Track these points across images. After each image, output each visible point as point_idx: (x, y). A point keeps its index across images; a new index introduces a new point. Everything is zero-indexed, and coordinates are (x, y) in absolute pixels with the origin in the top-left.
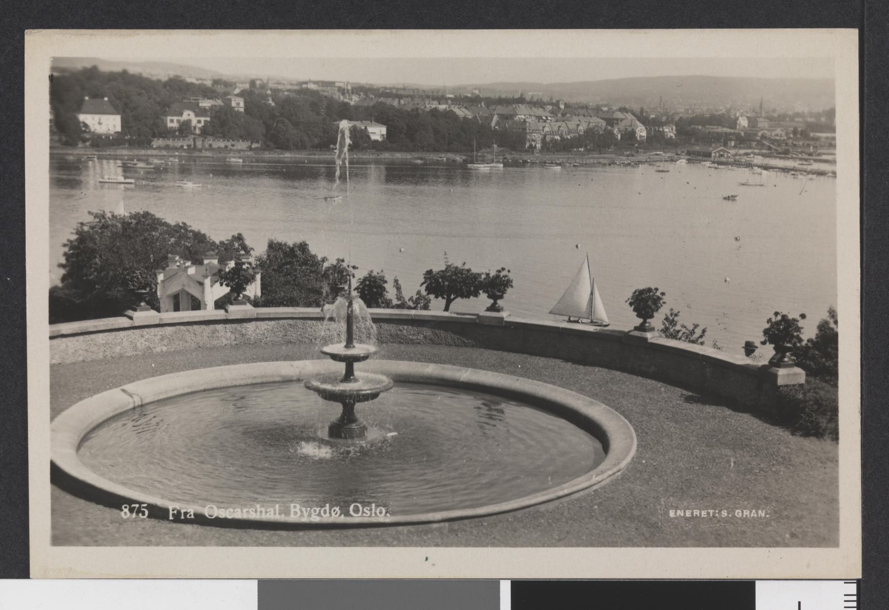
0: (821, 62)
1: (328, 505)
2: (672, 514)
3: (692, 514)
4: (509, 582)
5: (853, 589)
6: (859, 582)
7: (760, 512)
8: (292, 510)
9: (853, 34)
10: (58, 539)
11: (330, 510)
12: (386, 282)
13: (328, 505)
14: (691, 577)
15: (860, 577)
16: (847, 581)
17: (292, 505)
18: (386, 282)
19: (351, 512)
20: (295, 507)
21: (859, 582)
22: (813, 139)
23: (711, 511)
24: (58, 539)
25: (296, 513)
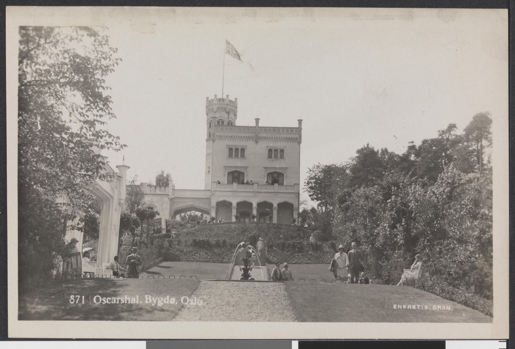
0: (16, 17)
1: (168, 297)
2: (395, 307)
3: (397, 307)
4: (297, 342)
5: (504, 345)
6: (507, 341)
7: (447, 307)
8: (147, 299)
9: (504, 12)
10: (21, 317)
11: (170, 299)
12: (72, 221)
13: (168, 297)
14: (426, 338)
15: (508, 338)
16: (501, 340)
17: (146, 296)
18: (72, 221)
19: (438, 190)
20: (148, 297)
21: (507, 341)
22: (168, 231)
23: (418, 306)
24: (21, 317)
25: (148, 300)
